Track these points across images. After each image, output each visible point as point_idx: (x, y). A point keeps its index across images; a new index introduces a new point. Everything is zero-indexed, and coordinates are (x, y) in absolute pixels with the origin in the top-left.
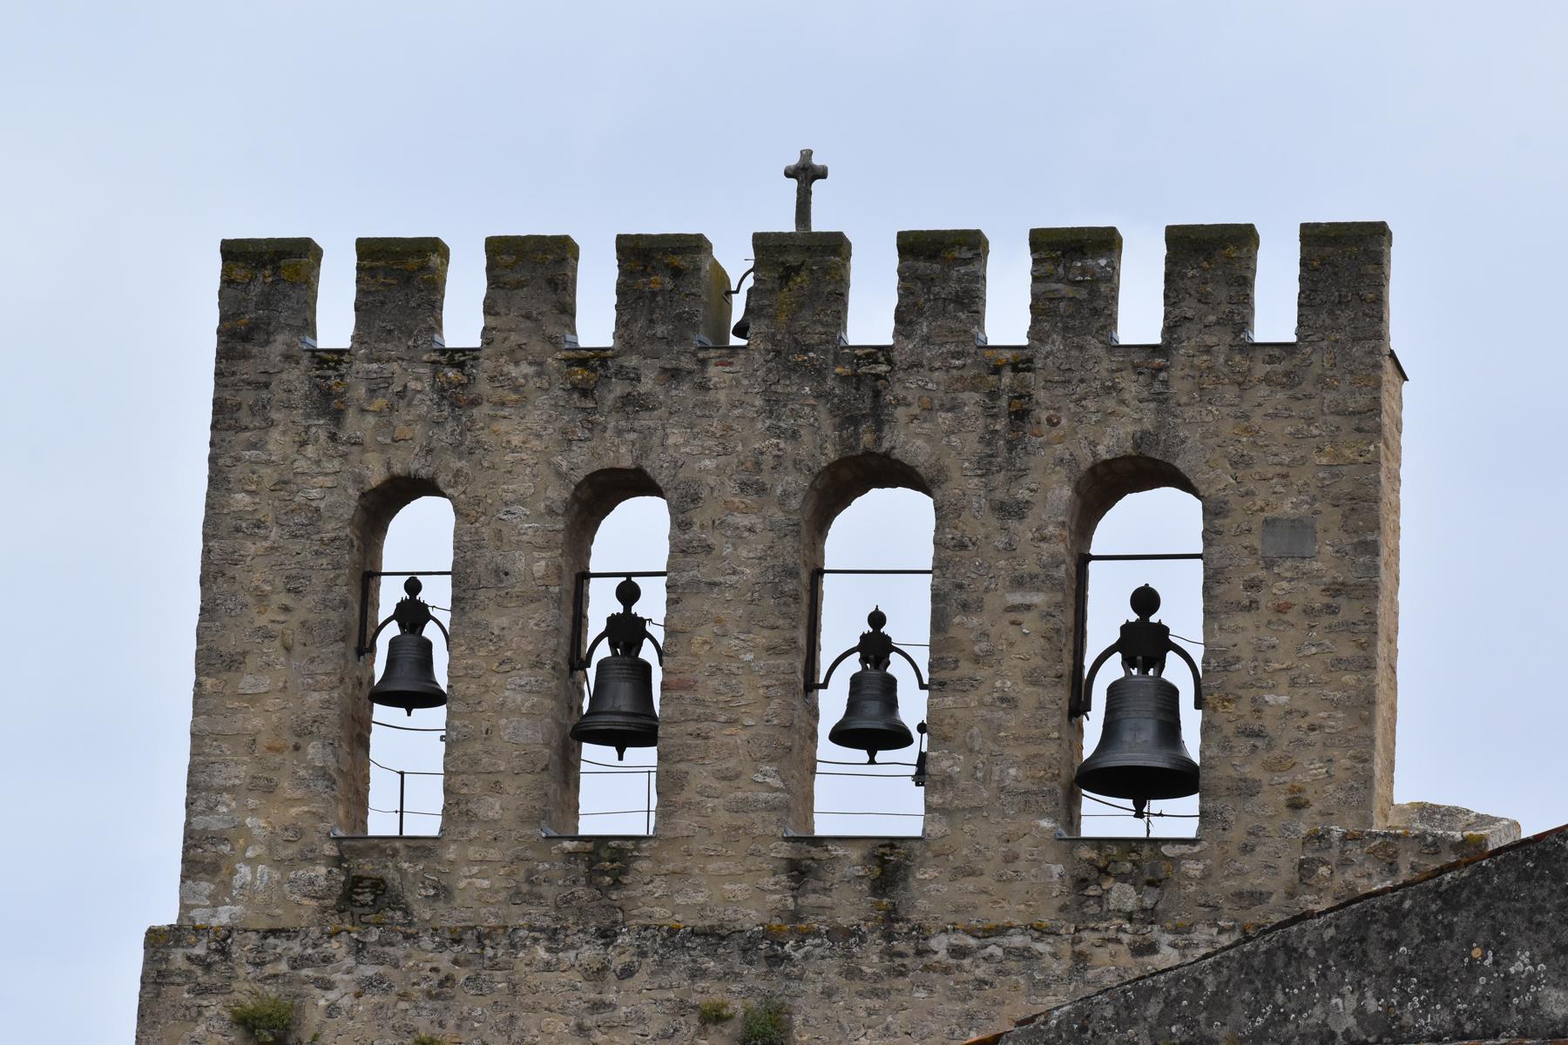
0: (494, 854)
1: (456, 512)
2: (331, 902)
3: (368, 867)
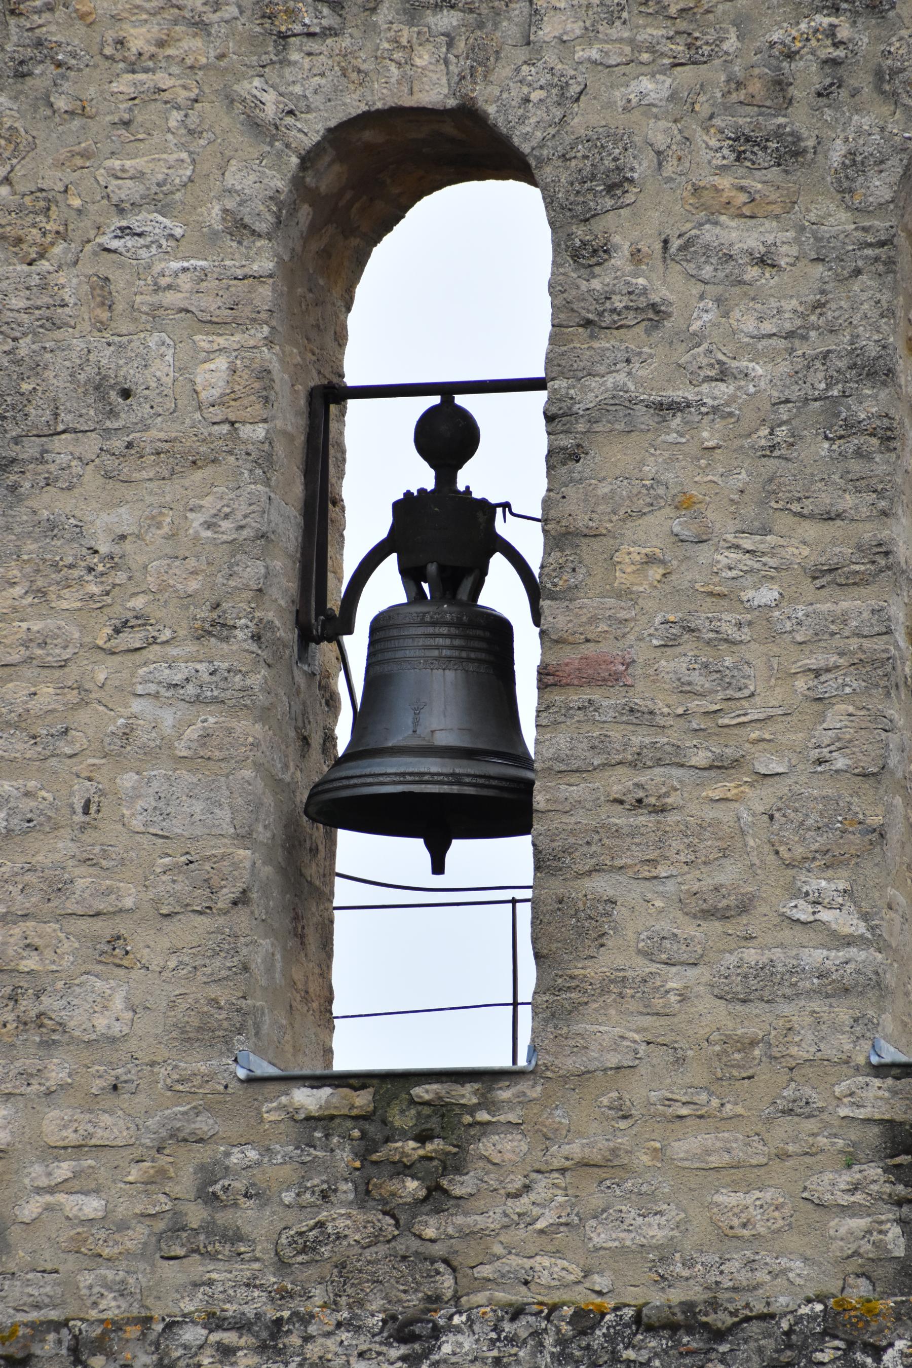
0: (111, 1127)
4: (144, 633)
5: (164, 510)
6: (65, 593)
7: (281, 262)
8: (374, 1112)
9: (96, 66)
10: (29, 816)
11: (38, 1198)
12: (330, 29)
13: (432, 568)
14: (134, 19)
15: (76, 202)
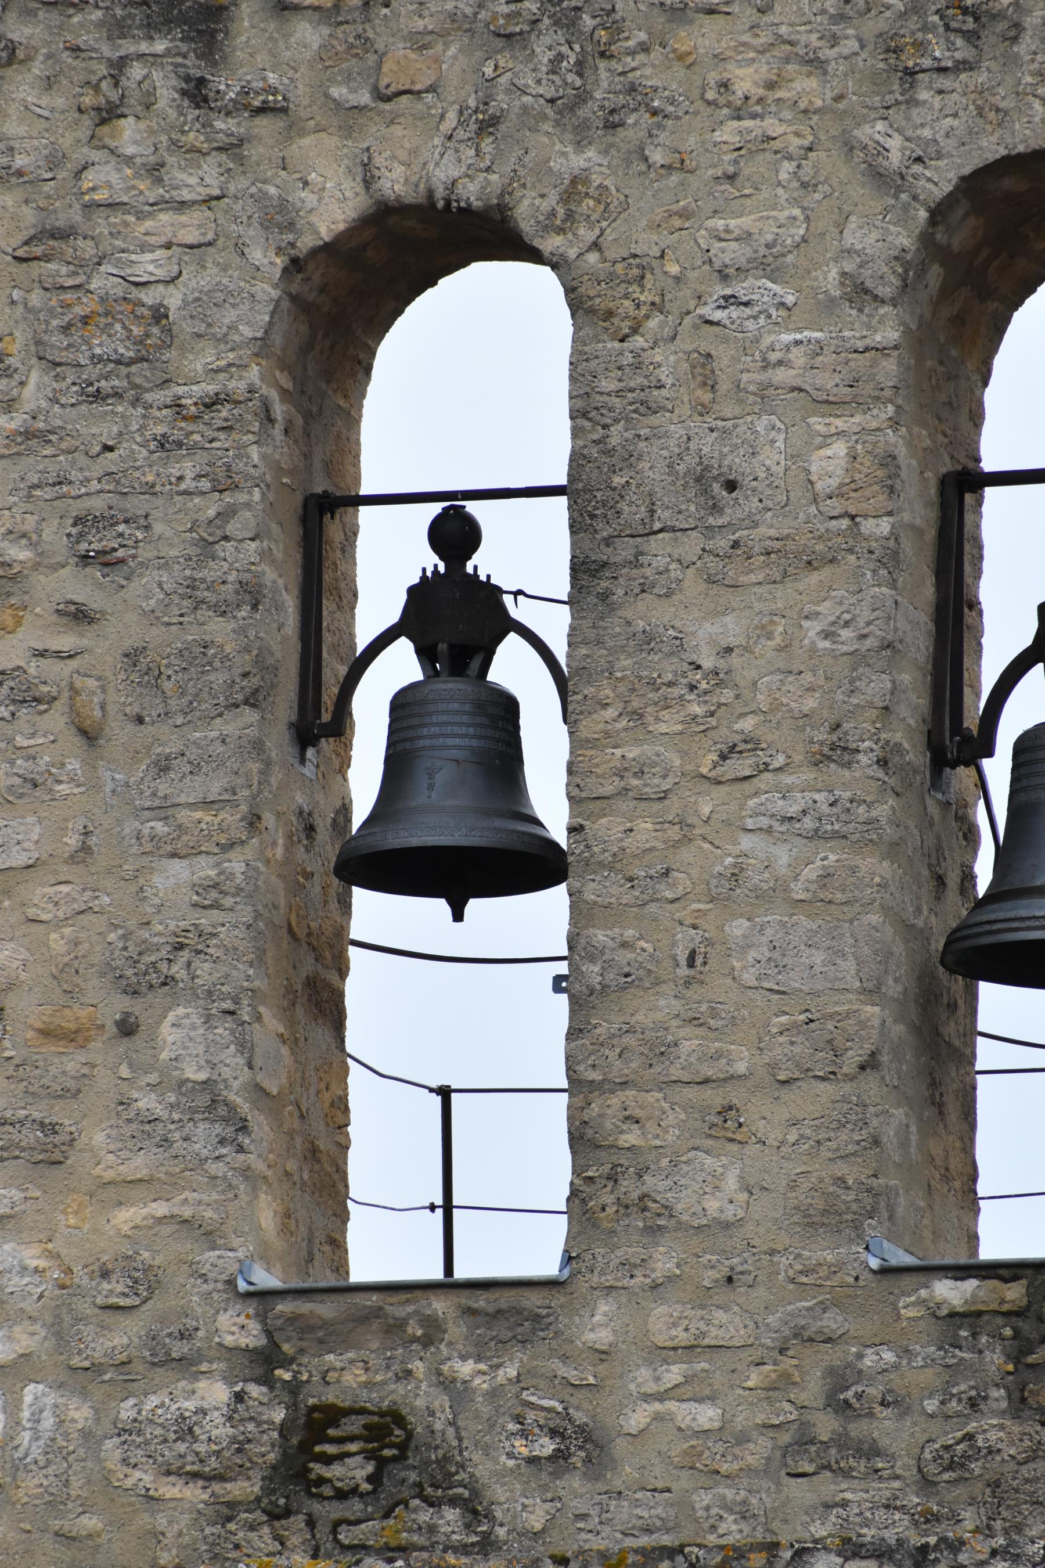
0: (726, 1325)
1: (577, 303)
2: (245, 1488)
3: (353, 1378)
4: (754, 759)
5: (775, 618)
6: (665, 714)
7: (907, 332)
8: (1028, 1307)
9: (696, 113)
10: (626, 970)
11: (645, 1406)
12: (965, 62)
13: (443, 647)
14: (740, 57)
15: (674, 269)
